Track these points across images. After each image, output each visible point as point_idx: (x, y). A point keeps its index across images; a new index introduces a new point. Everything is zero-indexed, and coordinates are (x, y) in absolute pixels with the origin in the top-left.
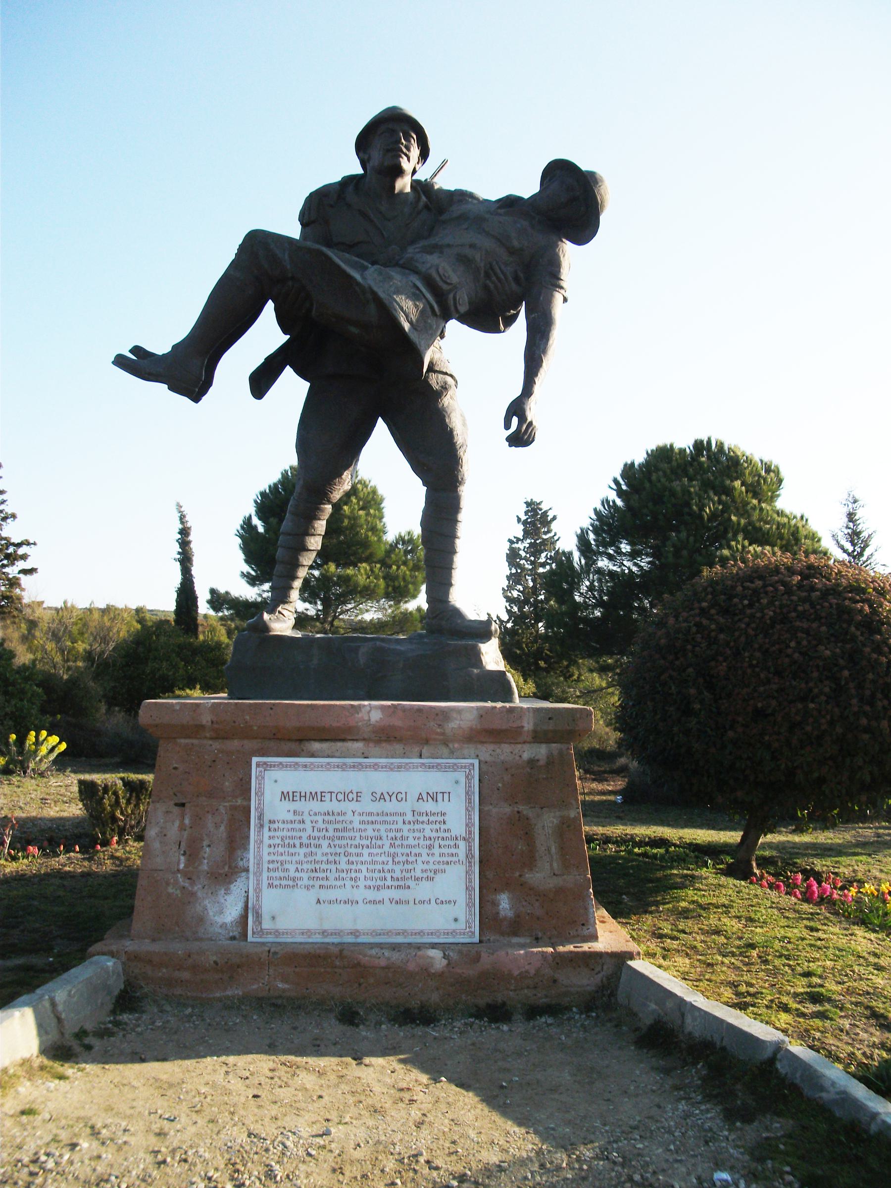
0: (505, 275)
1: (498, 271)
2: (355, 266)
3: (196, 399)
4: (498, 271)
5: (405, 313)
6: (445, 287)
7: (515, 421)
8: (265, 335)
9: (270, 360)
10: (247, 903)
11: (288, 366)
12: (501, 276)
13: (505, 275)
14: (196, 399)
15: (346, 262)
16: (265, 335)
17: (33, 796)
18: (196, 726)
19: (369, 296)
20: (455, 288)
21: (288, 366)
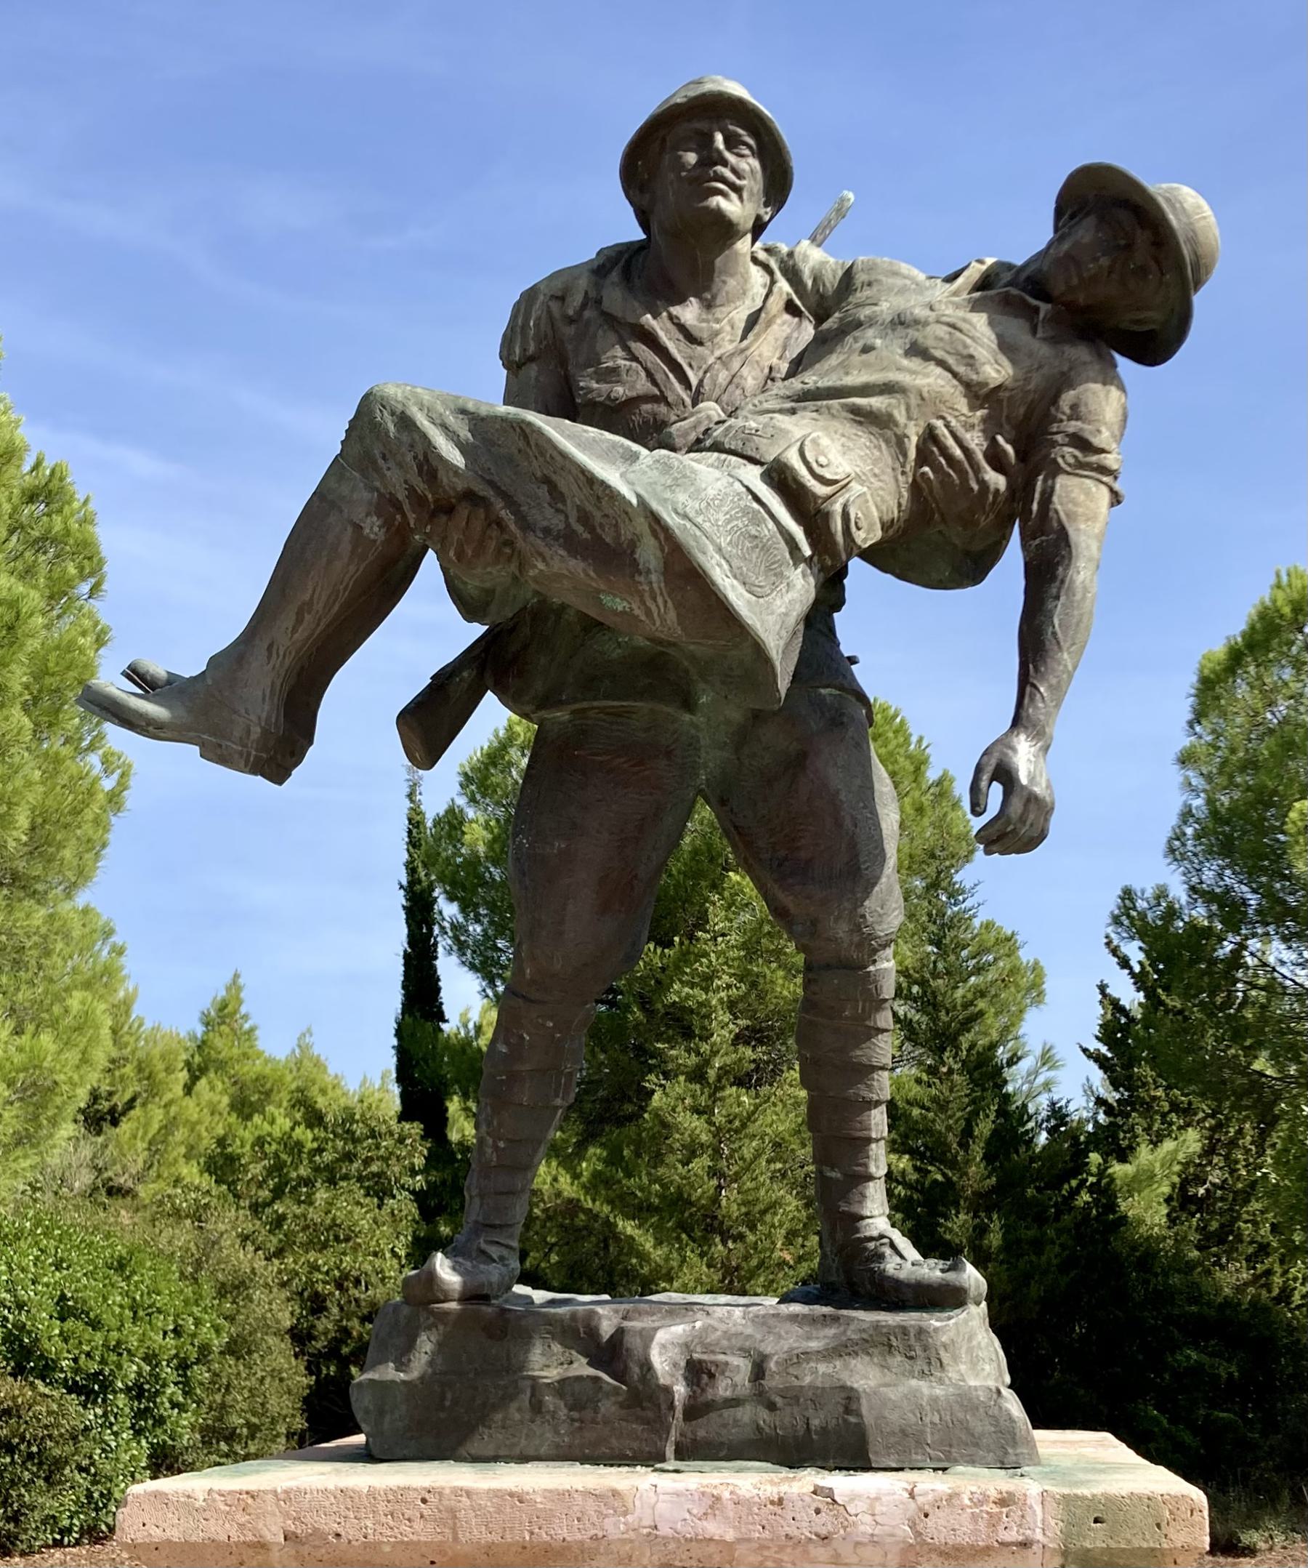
0: (965, 450)
1: (950, 442)
2: (608, 454)
3: (278, 773)
4: (950, 442)
5: (712, 542)
6: (821, 490)
7: (995, 793)
8: (426, 628)
9: (442, 680)
10: (961, 331)
11: (489, 693)
12: (958, 452)
13: (965, 450)
14: (278, 773)
15: (585, 445)
16: (426, 628)
17: (217, 1343)
18: (1056, 343)
19: (642, 525)
20: (839, 485)
21: (489, 693)
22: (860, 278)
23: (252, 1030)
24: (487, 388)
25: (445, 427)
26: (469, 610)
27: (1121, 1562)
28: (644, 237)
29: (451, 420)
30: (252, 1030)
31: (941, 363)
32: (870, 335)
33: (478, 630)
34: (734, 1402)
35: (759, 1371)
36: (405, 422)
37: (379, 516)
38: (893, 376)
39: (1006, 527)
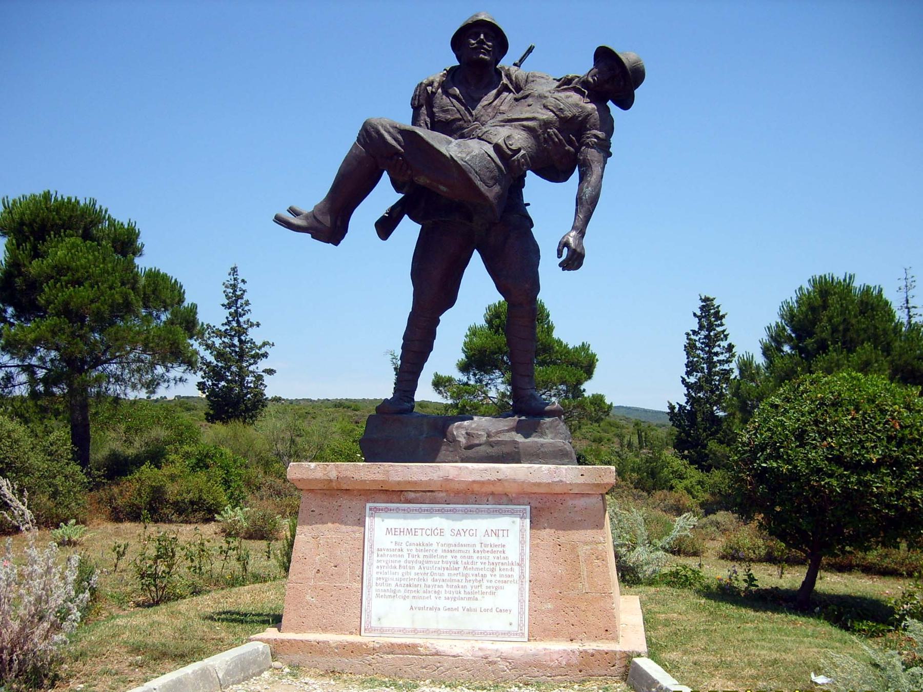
3: (336, 243)
8: (384, 195)
14: (336, 243)
16: (384, 195)
22: (531, 79)
23: (176, 280)
24: (404, 119)
25: (389, 132)
26: (398, 189)
27: (399, 363)
28: (458, 64)
29: (391, 130)
30: (176, 280)
31: (551, 111)
32: (530, 100)
33: (401, 196)
34: (480, 445)
35: (489, 436)
36: (378, 132)
37: (371, 158)
38: (536, 115)
39: (128, 519)
